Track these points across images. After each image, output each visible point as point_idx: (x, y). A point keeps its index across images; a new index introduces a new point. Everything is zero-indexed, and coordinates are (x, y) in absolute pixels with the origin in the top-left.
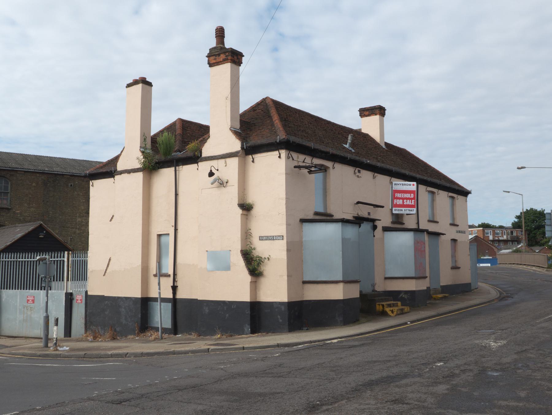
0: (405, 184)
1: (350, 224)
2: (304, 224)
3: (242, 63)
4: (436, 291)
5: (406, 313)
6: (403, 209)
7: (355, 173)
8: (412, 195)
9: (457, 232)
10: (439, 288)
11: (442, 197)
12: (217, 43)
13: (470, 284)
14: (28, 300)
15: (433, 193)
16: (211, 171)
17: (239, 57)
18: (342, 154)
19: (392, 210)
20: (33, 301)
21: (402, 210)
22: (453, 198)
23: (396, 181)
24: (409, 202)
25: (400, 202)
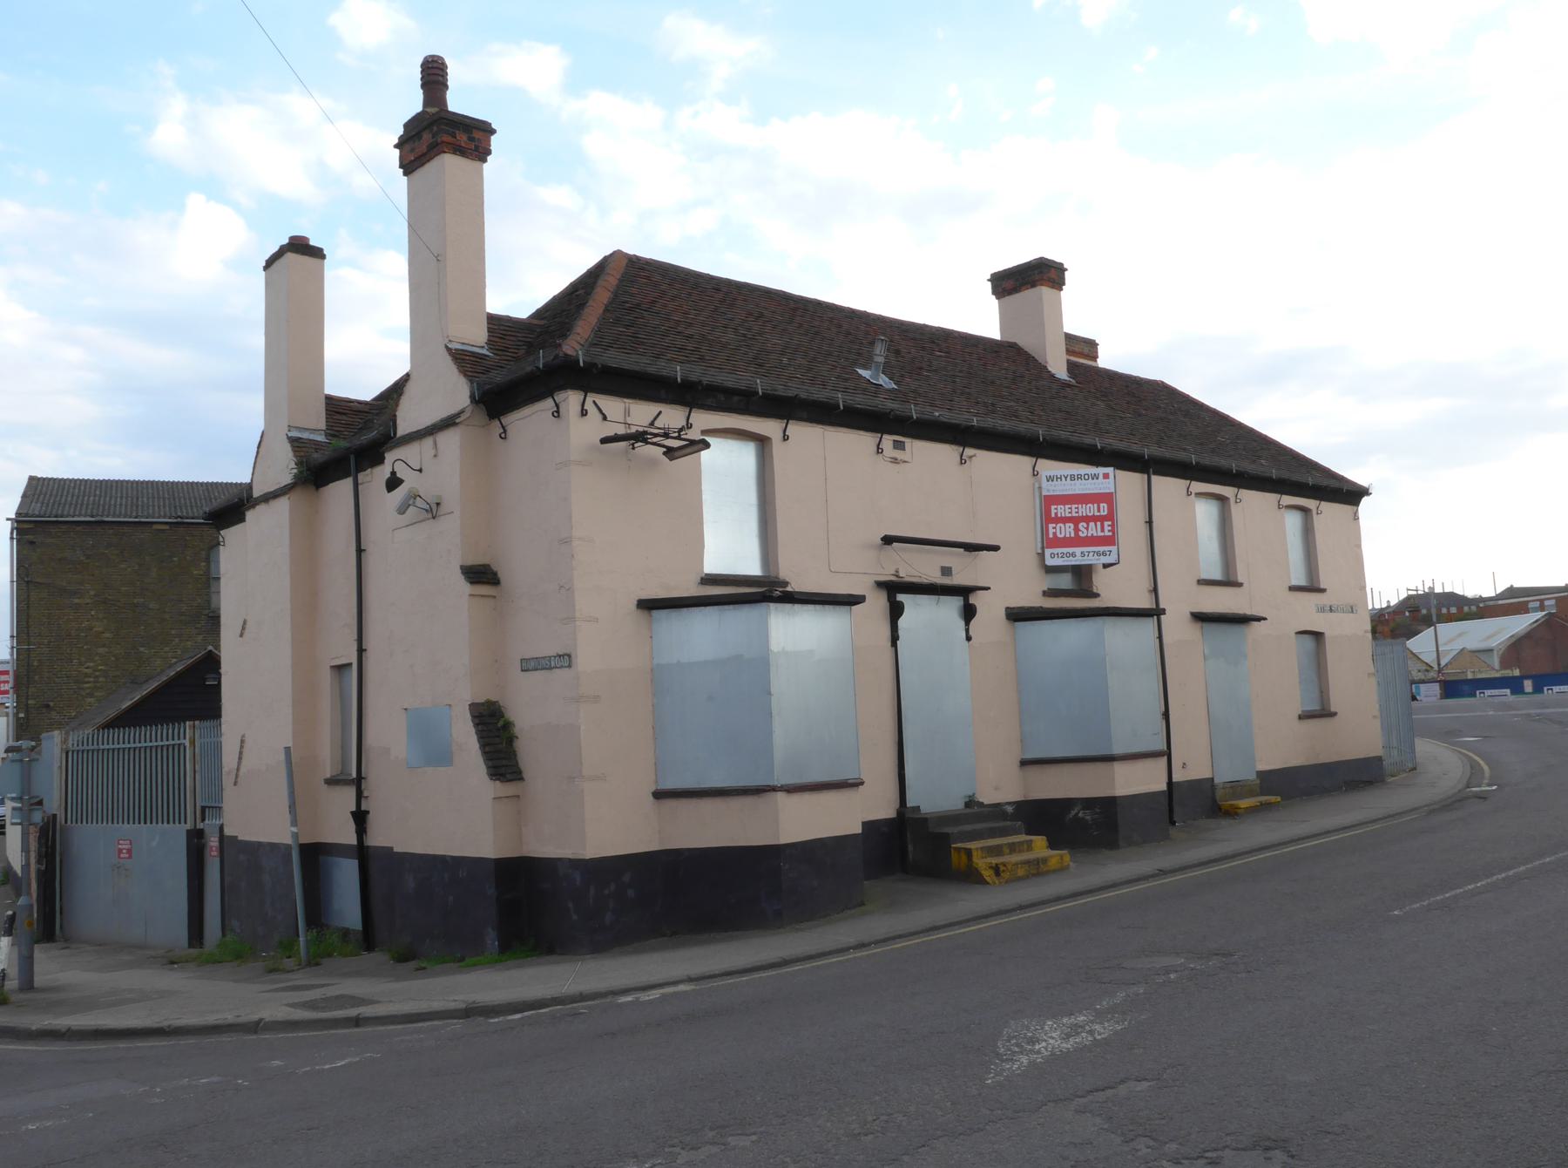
0: (1079, 477)
1: (810, 607)
2: (655, 613)
3: (489, 152)
4: (1237, 788)
5: (1054, 871)
6: (1078, 550)
7: (879, 450)
8: (1104, 506)
9: (1322, 610)
10: (1253, 776)
11: (1256, 509)
12: (426, 103)
13: (1379, 759)
14: (120, 851)
15: (1222, 499)
16: (393, 473)
17: (477, 134)
18: (860, 401)
19: (1042, 556)
20: (129, 851)
21: (1073, 555)
22: (1222, 499)
23: (1048, 467)
24: (1094, 530)
25: (1067, 530)
